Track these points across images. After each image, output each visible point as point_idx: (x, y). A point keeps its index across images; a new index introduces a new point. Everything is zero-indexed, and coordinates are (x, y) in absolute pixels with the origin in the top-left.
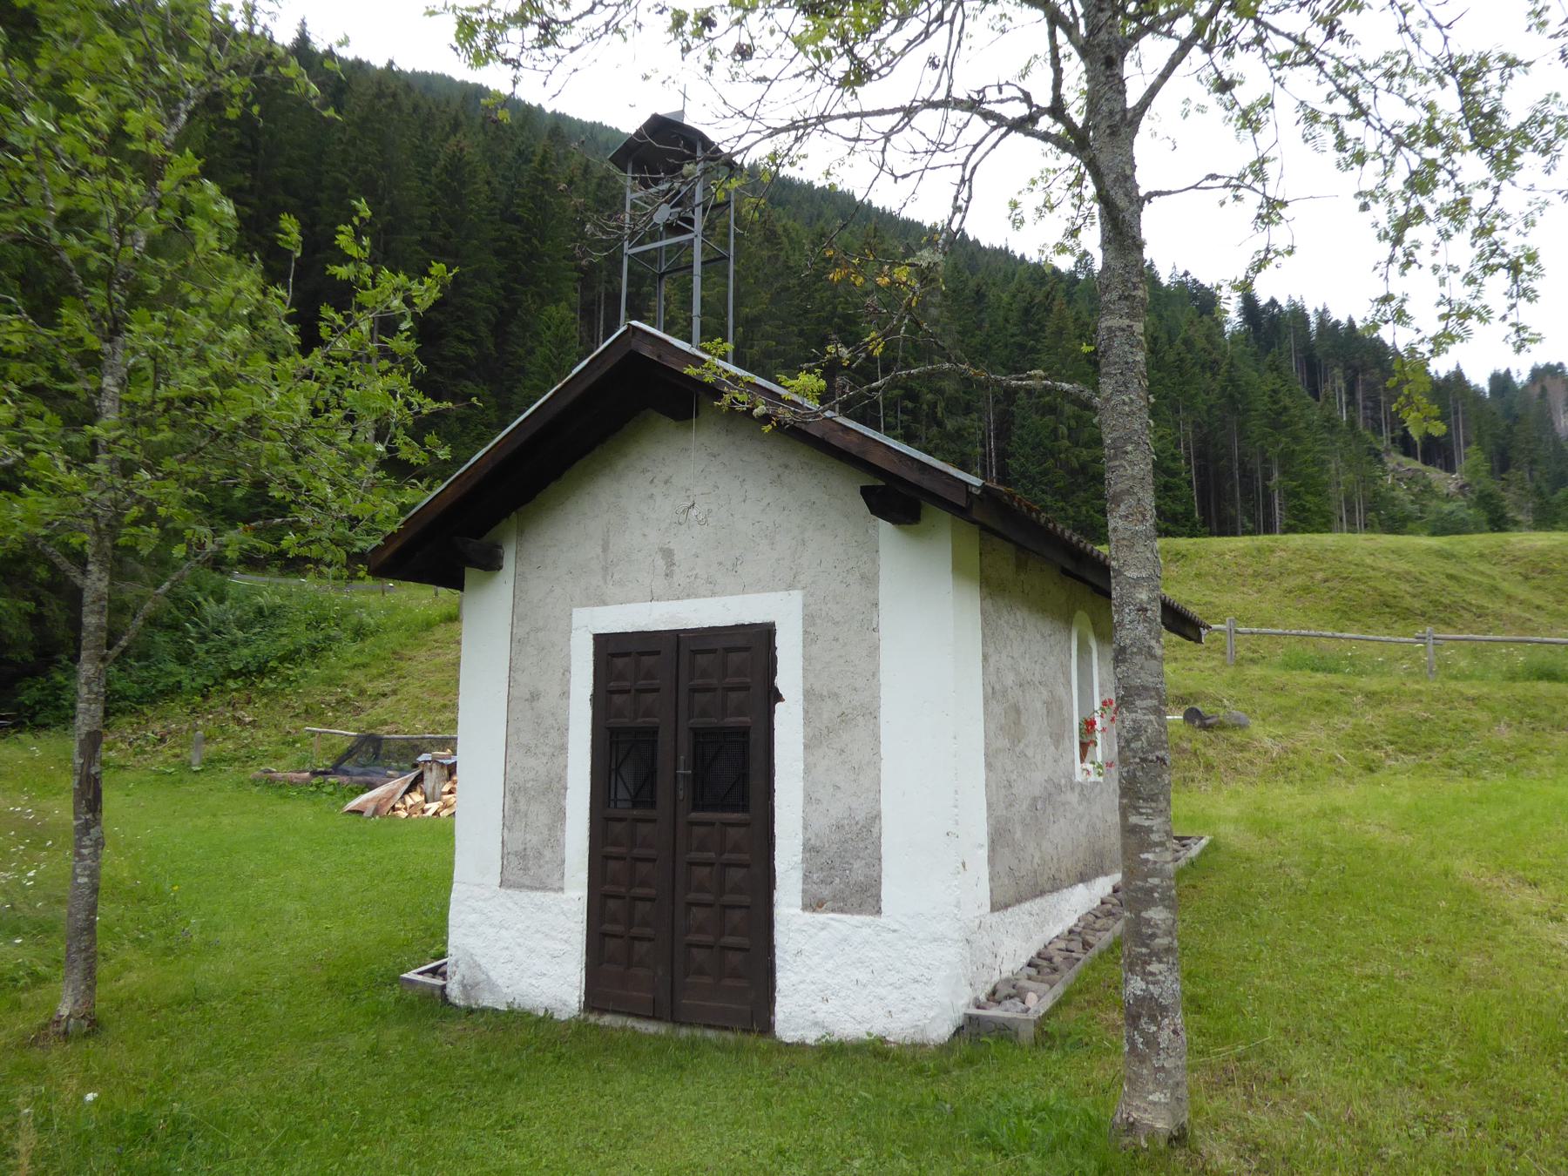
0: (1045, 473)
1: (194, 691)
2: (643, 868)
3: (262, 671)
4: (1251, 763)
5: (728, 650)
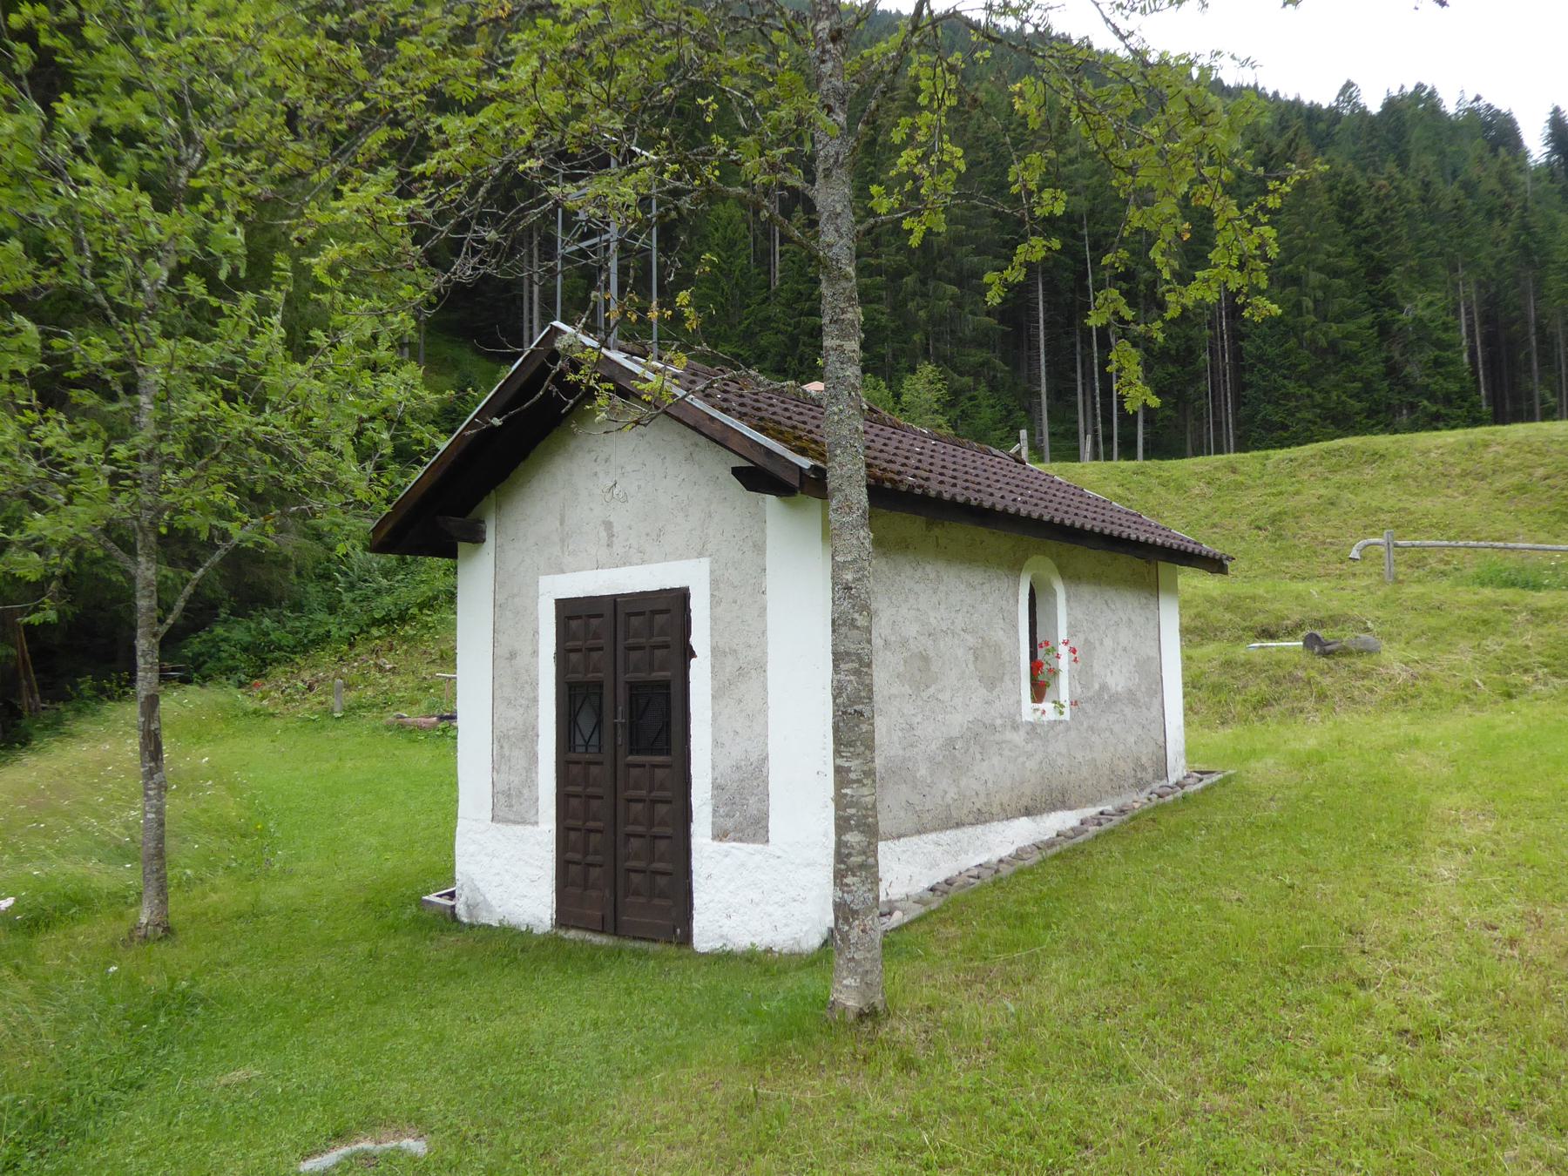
0: (1286, 354)
1: (341, 640)
2: (595, 804)
3: (403, 618)
4: (1371, 691)
5: (654, 612)
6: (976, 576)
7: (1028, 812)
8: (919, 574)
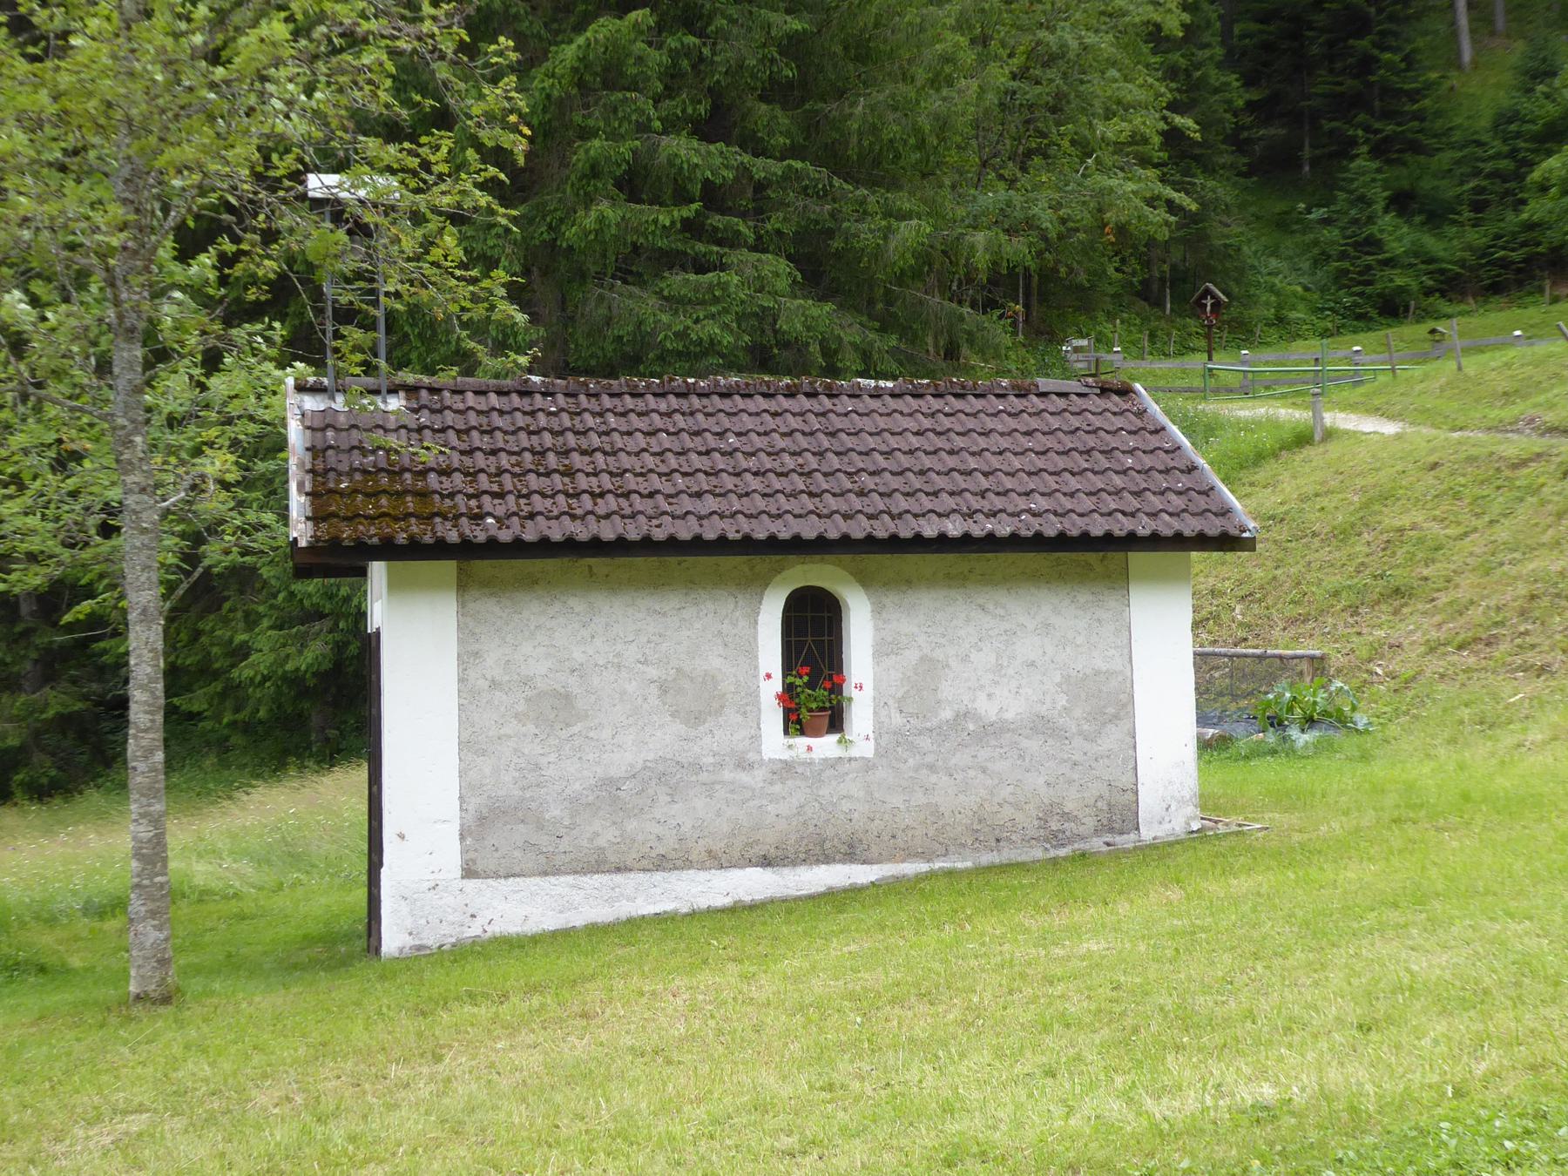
6: (670, 603)
7: (766, 862)
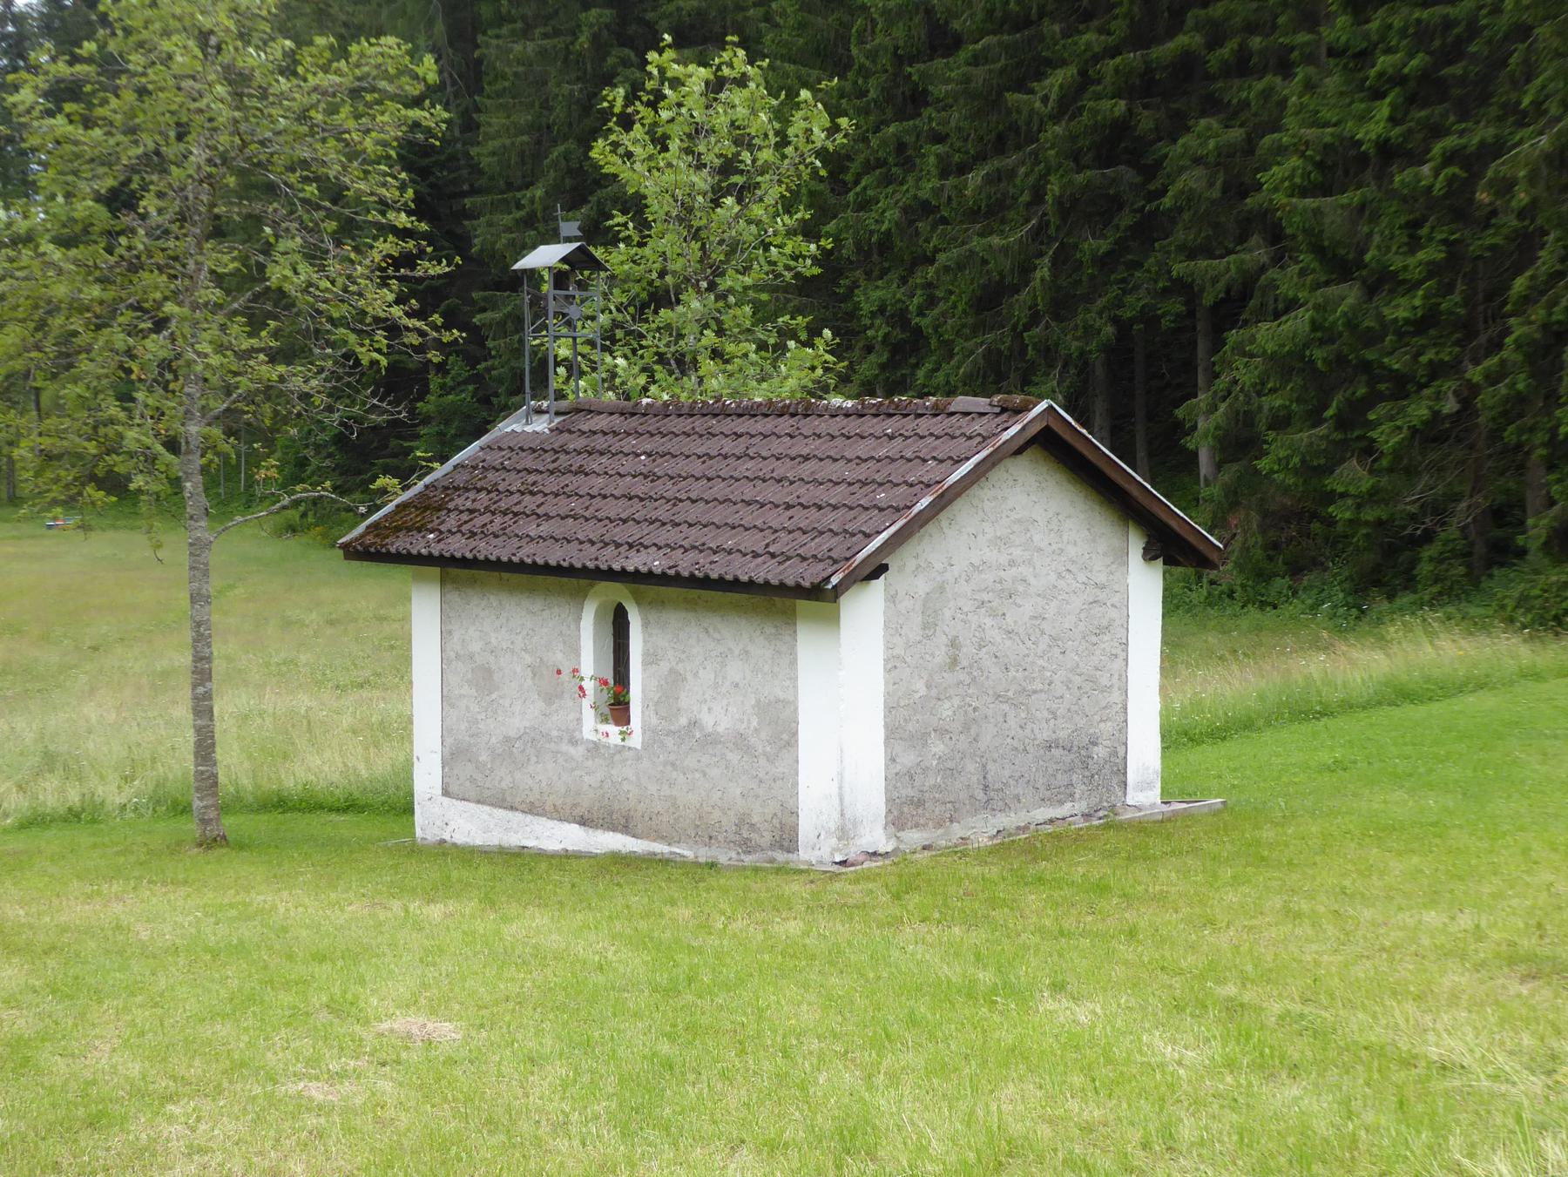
6: (537, 604)
7: (583, 822)
8: (484, 603)
